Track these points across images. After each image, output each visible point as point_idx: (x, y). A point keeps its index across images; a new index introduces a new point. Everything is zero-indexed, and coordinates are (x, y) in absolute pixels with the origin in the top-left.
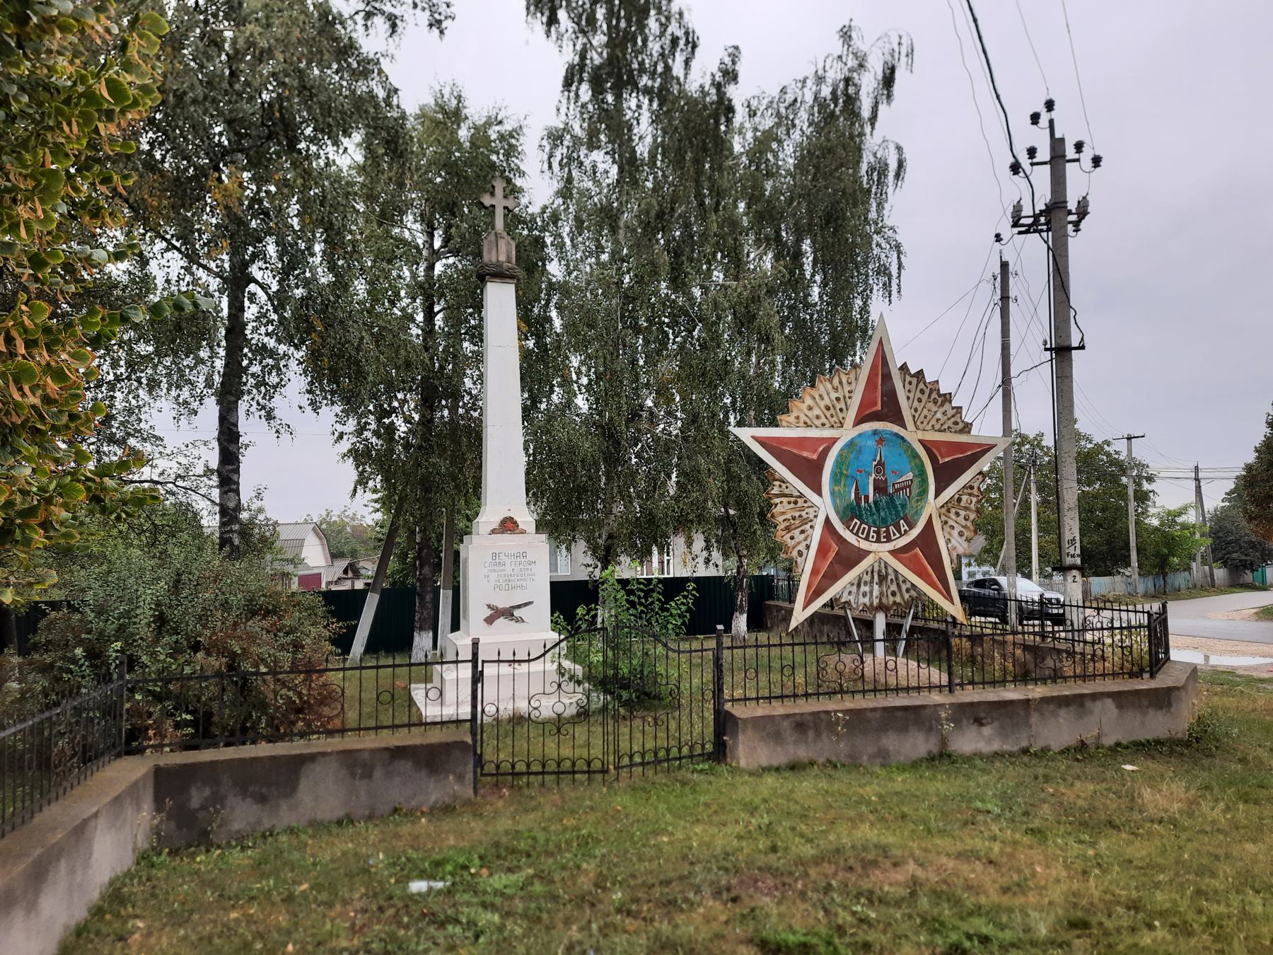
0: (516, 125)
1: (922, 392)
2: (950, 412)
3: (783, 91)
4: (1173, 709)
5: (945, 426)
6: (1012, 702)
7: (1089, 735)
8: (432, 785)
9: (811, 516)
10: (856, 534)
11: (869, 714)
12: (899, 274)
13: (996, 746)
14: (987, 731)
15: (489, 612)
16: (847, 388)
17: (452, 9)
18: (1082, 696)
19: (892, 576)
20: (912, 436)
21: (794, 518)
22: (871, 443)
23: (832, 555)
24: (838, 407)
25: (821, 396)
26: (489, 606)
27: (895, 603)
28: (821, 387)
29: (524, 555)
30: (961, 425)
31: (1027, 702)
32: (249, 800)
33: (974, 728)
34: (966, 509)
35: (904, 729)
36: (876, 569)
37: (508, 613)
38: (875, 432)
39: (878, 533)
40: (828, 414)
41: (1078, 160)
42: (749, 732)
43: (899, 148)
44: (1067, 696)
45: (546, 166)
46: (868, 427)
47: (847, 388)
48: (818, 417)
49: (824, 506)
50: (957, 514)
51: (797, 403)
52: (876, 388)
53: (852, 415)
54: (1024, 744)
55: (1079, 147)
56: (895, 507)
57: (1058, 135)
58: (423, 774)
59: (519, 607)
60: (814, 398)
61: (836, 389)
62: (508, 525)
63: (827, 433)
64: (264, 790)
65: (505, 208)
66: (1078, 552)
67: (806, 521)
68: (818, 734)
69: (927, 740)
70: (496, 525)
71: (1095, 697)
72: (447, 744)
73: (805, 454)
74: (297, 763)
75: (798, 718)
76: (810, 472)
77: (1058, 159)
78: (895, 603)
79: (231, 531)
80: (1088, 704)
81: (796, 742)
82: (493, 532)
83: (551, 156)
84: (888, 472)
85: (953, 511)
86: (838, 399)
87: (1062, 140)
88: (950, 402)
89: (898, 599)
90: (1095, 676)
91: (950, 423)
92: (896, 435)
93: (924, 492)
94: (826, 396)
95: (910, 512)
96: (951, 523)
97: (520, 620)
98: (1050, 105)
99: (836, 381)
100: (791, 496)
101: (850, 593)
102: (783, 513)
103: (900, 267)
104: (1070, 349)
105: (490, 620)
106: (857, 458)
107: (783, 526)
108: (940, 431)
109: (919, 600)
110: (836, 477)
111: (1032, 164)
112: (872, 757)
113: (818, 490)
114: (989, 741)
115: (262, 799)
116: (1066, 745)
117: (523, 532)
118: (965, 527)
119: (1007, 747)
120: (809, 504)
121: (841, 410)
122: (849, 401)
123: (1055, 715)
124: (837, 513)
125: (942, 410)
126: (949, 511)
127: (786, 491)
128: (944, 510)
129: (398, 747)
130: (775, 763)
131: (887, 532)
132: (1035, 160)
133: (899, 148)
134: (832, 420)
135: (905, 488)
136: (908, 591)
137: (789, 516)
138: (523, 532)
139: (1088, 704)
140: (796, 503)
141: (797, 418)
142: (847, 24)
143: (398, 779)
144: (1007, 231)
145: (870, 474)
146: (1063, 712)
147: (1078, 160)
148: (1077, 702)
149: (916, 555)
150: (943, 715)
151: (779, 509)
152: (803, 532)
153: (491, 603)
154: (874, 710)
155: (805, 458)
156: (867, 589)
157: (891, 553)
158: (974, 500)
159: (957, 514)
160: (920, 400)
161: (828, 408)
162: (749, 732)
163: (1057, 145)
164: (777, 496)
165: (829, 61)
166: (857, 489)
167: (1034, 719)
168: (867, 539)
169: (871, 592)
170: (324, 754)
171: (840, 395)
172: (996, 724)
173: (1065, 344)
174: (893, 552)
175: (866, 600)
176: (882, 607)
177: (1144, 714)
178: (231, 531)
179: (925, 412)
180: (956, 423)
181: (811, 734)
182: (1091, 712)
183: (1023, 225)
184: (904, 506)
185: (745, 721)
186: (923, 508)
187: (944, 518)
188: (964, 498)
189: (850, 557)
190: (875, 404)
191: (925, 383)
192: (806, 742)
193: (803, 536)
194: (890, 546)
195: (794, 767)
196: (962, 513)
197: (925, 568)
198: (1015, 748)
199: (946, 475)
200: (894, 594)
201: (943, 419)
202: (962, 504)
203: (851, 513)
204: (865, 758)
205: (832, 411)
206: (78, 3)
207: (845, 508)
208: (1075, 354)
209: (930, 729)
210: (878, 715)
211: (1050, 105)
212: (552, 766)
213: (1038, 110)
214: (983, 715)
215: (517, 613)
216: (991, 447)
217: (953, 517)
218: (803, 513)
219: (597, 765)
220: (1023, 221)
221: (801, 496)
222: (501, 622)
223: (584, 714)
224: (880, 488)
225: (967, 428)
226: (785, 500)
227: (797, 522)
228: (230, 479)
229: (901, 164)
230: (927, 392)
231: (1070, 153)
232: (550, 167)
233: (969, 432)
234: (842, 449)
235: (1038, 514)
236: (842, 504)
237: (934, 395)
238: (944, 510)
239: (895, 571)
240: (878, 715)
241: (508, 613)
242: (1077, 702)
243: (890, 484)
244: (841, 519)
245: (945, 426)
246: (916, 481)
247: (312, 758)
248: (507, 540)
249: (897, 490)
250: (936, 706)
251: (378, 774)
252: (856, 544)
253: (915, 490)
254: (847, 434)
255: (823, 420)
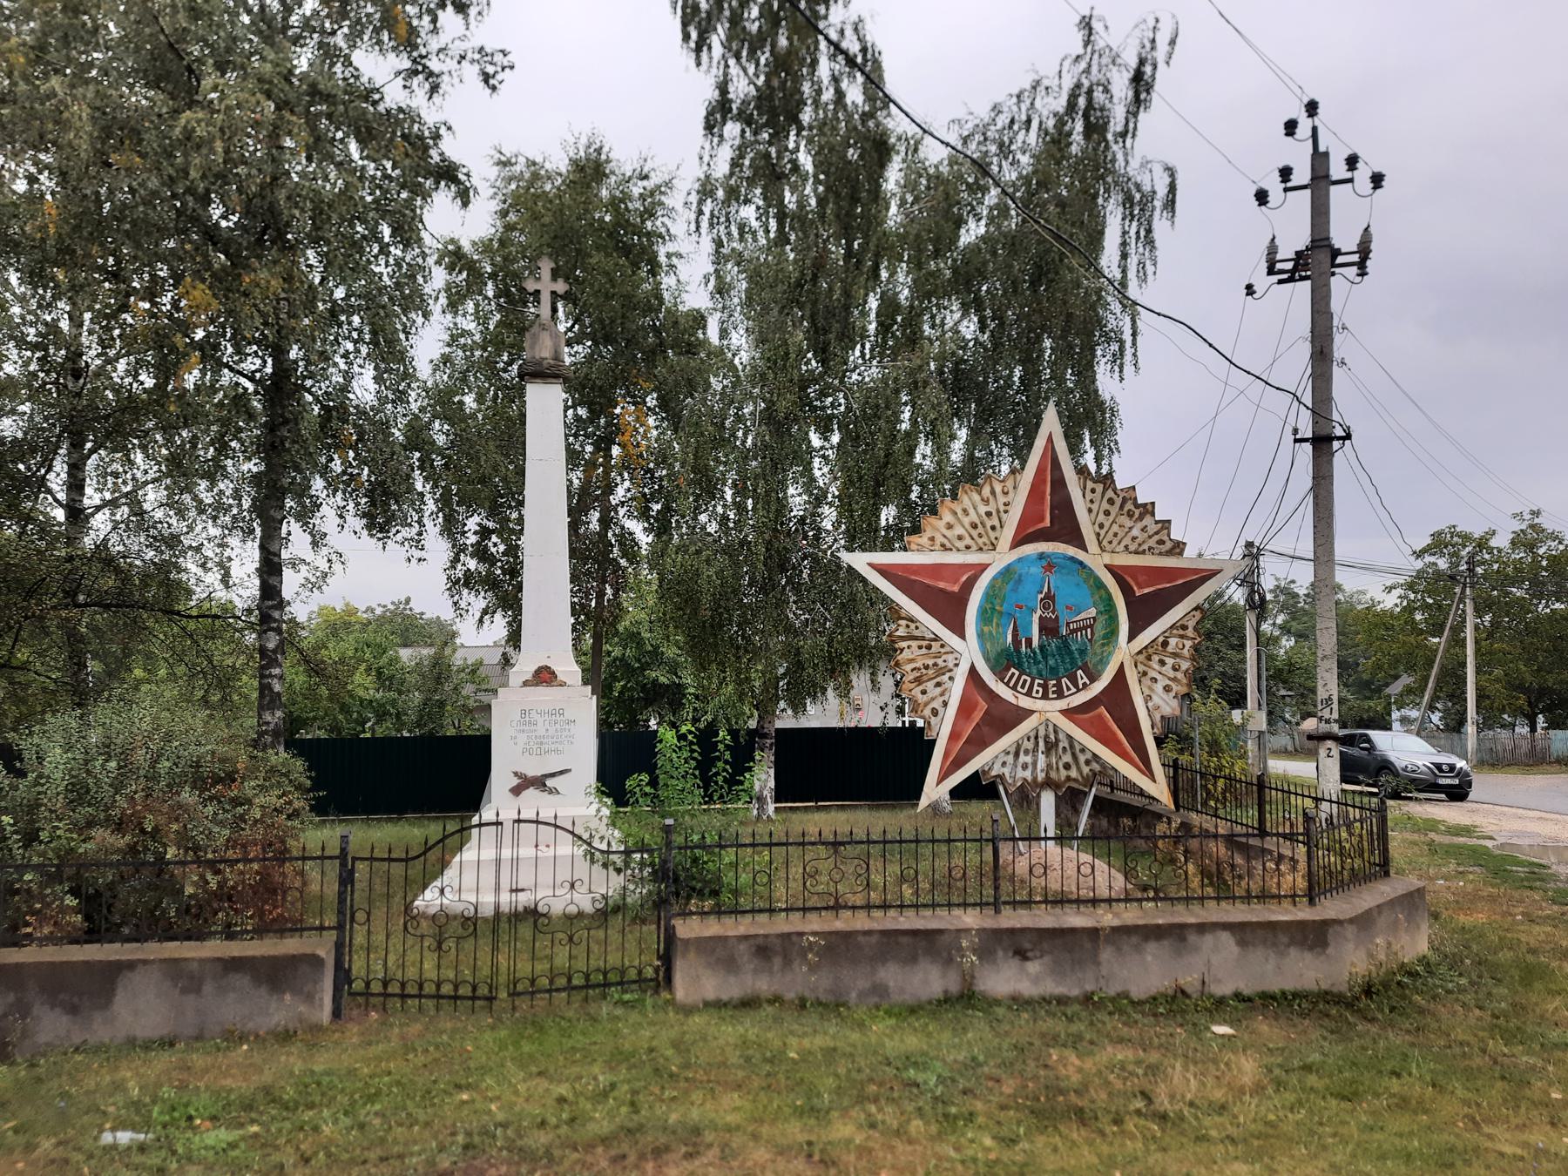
0: (667, 178)
1: (1111, 502)
2: (1153, 528)
3: (997, 109)
4: (1330, 950)
5: (1145, 547)
6: (1073, 931)
7: (1190, 981)
8: (274, 1005)
9: (951, 665)
10: (1014, 688)
11: (861, 938)
12: (1134, 343)
13: (1051, 987)
14: (1033, 967)
15: (515, 781)
16: (1002, 499)
17: (509, 57)
18: (1183, 927)
19: (1064, 743)
20: (1095, 560)
21: (927, 667)
22: (1036, 570)
23: (978, 716)
24: (989, 524)
25: (965, 511)
26: (516, 774)
27: (1068, 778)
28: (965, 499)
29: (561, 713)
30: (1169, 545)
31: (1094, 933)
32: (58, 1010)
33: (1015, 963)
34: (1175, 655)
35: (913, 960)
36: (1042, 733)
37: (539, 783)
38: (1041, 556)
39: (1045, 687)
40: (975, 533)
41: (1350, 180)
42: (692, 955)
43: (1171, 172)
44: (1158, 926)
45: (693, 227)
46: (1031, 549)
47: (1002, 499)
48: (960, 538)
49: (968, 651)
50: (1162, 663)
51: (932, 520)
52: (1043, 498)
53: (1008, 534)
54: (1089, 987)
55: (1352, 162)
56: (1070, 653)
57: (1322, 149)
58: (263, 990)
59: (553, 775)
60: (955, 513)
61: (986, 501)
62: (544, 676)
63: (973, 558)
64: (76, 1000)
65: (553, 293)
66: (1335, 716)
67: (942, 671)
68: (787, 962)
69: (944, 976)
70: (529, 676)
71: (1202, 928)
72: (294, 956)
73: (942, 585)
74: (115, 970)
75: (760, 941)
76: (950, 609)
77: (1321, 180)
78: (1068, 778)
79: (270, 676)
80: (1192, 938)
81: (755, 971)
82: (526, 684)
83: (700, 213)
84: (1060, 606)
85: (1156, 658)
86: (989, 514)
87: (1326, 154)
88: (1153, 514)
89: (1074, 773)
90: (1279, 897)
91: (1152, 542)
92: (1072, 559)
93: (1112, 633)
94: (971, 511)
95: (1091, 660)
96: (1152, 674)
97: (553, 791)
98: (1312, 108)
99: (986, 491)
100: (923, 638)
101: (1004, 764)
102: (912, 660)
103: (1134, 335)
104: (1330, 439)
105: (516, 791)
106: (1015, 590)
107: (911, 676)
108: (1136, 552)
109: (1105, 774)
110: (985, 615)
111: (1286, 190)
112: (862, 995)
113: (960, 632)
114: (1036, 980)
115: (73, 1010)
116: (1153, 991)
117: (562, 684)
118: (1174, 679)
119: (1060, 990)
120: (947, 649)
121: (993, 528)
122: (1004, 516)
123: (1138, 949)
124: (987, 660)
125: (1140, 525)
126: (1149, 658)
127: (916, 633)
128: (1141, 658)
129: (233, 958)
130: (725, 997)
131: (1059, 685)
132: (1289, 185)
133: (1171, 172)
134: (980, 541)
135: (1085, 628)
136: (1087, 762)
137: (919, 664)
138: (562, 684)
139: (1192, 938)
140: (929, 647)
141: (932, 539)
142: (1087, 13)
143: (232, 995)
144: (1262, 281)
145: (1033, 610)
146: (1152, 947)
147: (1350, 180)
148: (1175, 934)
149: (1100, 717)
150: (965, 944)
151: (906, 655)
152: (938, 685)
153: (519, 770)
154: (868, 933)
155: (941, 590)
156: (1028, 759)
157: (1065, 713)
158: (1188, 644)
159: (1162, 663)
160: (1107, 513)
161: (975, 526)
162: (692, 955)
163: (1320, 159)
164: (903, 638)
165: (1067, 64)
166: (1015, 630)
167: (1106, 954)
168: (1029, 694)
169: (1035, 764)
170: (145, 962)
171: (992, 508)
172: (1047, 959)
173: (1324, 432)
174: (1067, 713)
175: (1028, 774)
176: (1049, 783)
177: (1282, 954)
178: (270, 676)
179: (1115, 528)
180: (1161, 542)
181: (777, 962)
182: (1197, 949)
183: (1282, 272)
184: (1082, 652)
185: (687, 942)
186: (1110, 654)
187: (1141, 668)
188: (1173, 641)
189: (1002, 719)
190: (1042, 519)
191: (1115, 490)
192: (771, 972)
193: (939, 690)
194: (1062, 704)
195: (748, 1003)
196: (1170, 661)
197: (1114, 734)
198: (1075, 992)
199: (1144, 612)
200: (1067, 767)
201: (1142, 537)
202: (1170, 649)
203: (1004, 662)
204: (854, 995)
205: (980, 529)
206: (734, 3)
207: (999, 655)
208: (1336, 444)
209: (949, 961)
210: (874, 939)
211: (1312, 108)
212: (429, 989)
213: (1293, 116)
214: (1027, 946)
215: (550, 783)
216: (1213, 574)
217: (1156, 666)
218: (940, 661)
219: (483, 990)
220: (1279, 266)
221: (937, 638)
222: (531, 793)
223: (607, 912)
224: (1048, 628)
225: (1178, 548)
226: (914, 644)
227: (931, 672)
228: (270, 617)
229: (1172, 188)
230: (1118, 502)
231: (1338, 169)
232: (698, 227)
233: (1181, 553)
234: (994, 579)
235: (1477, 642)
236: (993, 651)
237: (1129, 506)
238: (1141, 658)
239: (1070, 737)
240: (874, 939)
241: (539, 783)
242: (1175, 934)
243: (1063, 622)
244: (993, 669)
245: (1145, 547)
246: (1102, 619)
247: (131, 965)
248: (543, 694)
249: (1075, 631)
250: (959, 931)
251: (208, 988)
252: (1013, 701)
253: (1100, 630)
254: (1002, 558)
255: (968, 541)
